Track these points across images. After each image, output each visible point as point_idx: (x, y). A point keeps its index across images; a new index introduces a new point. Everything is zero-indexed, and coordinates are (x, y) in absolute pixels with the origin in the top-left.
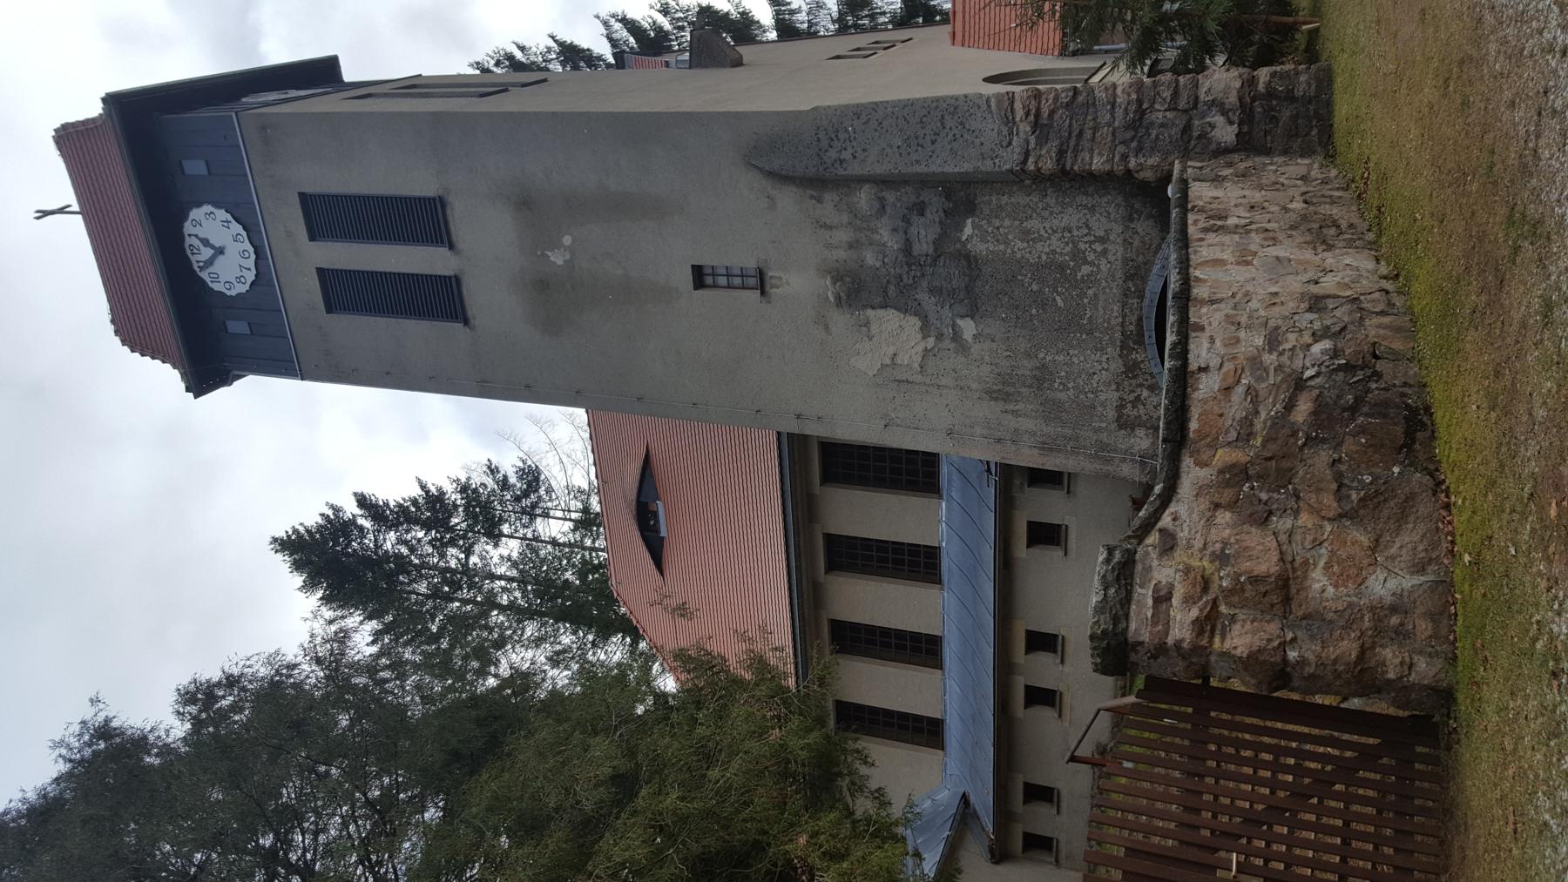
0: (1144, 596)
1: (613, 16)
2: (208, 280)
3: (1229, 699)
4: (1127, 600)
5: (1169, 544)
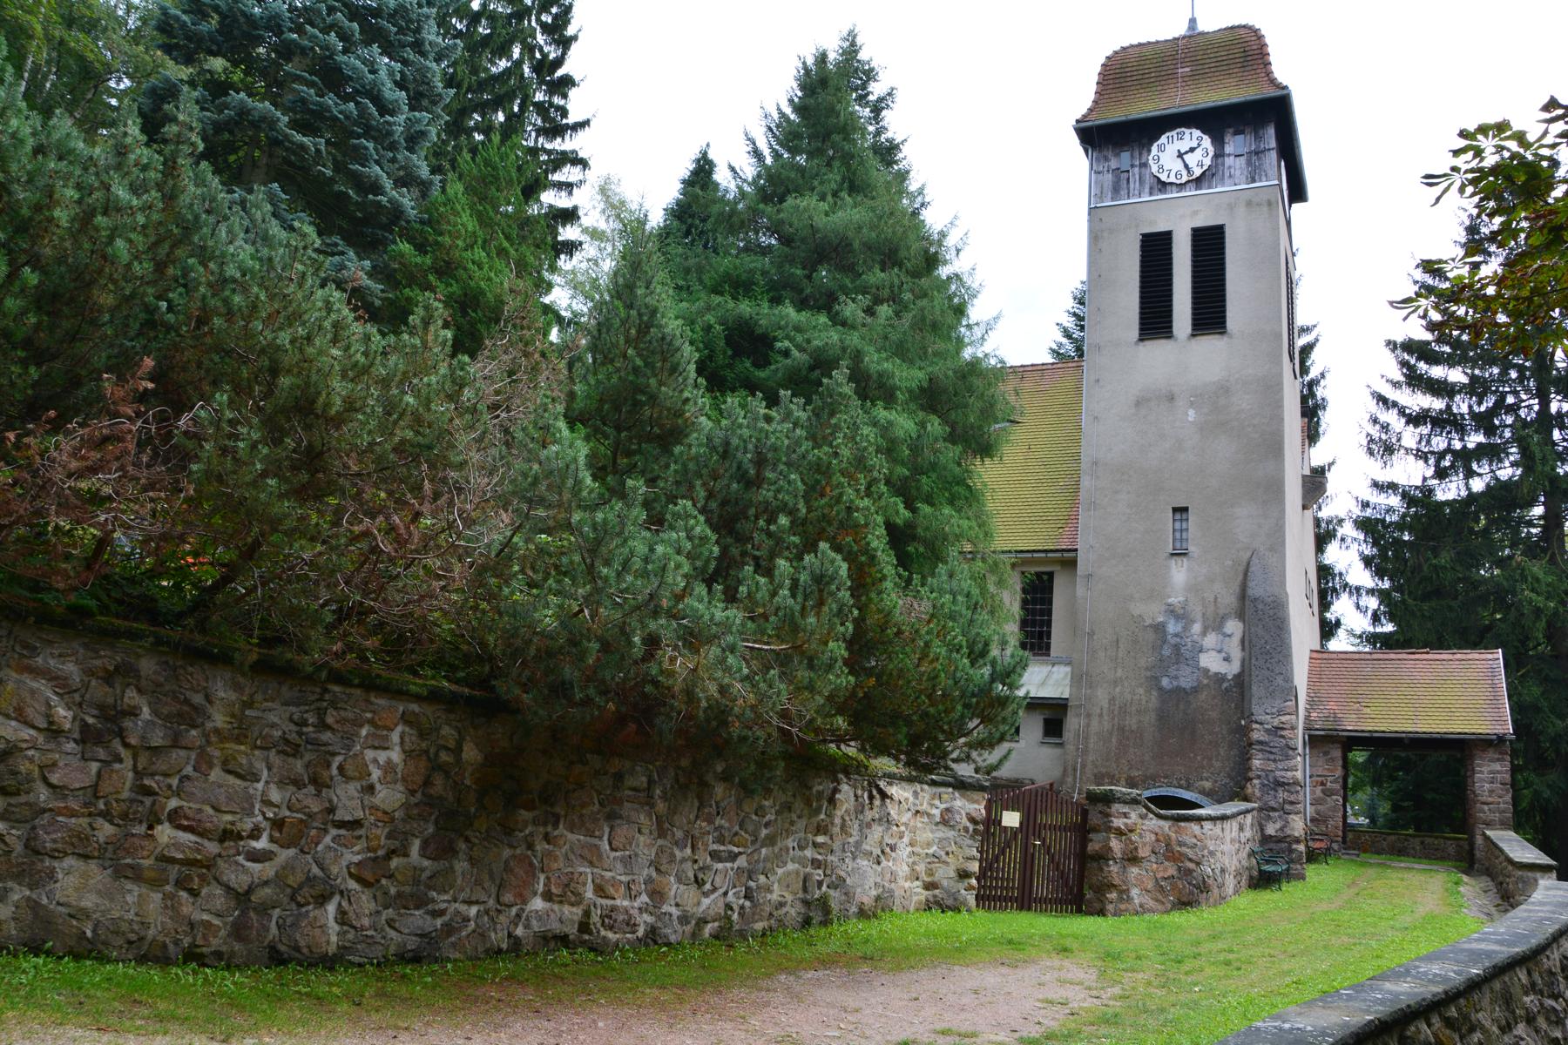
0: (1126, 809)
3: (1084, 841)
4: (1125, 802)
5: (1143, 817)
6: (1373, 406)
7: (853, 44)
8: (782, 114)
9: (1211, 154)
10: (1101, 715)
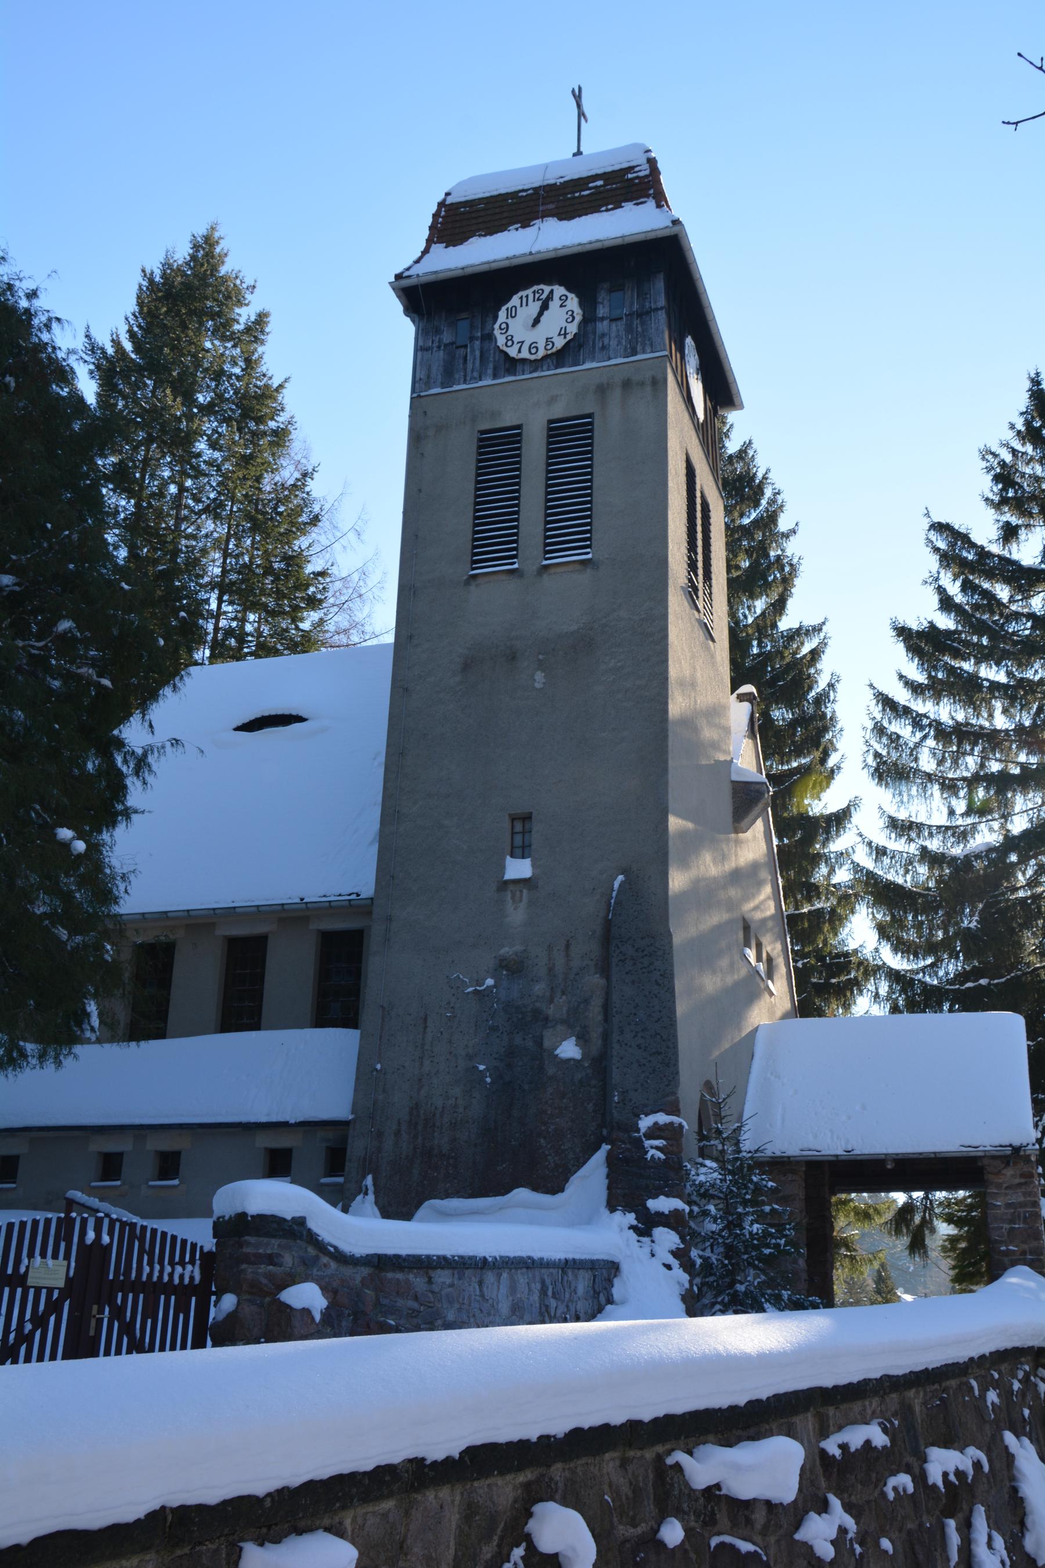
1: (824, 644)
2: (509, 305)
6: (877, 711)
7: (209, 255)
8: (116, 343)
9: (578, 318)
10: (398, 1133)
